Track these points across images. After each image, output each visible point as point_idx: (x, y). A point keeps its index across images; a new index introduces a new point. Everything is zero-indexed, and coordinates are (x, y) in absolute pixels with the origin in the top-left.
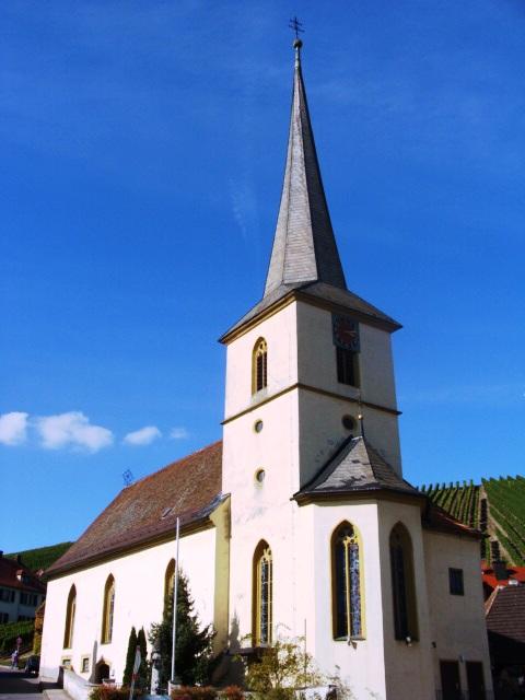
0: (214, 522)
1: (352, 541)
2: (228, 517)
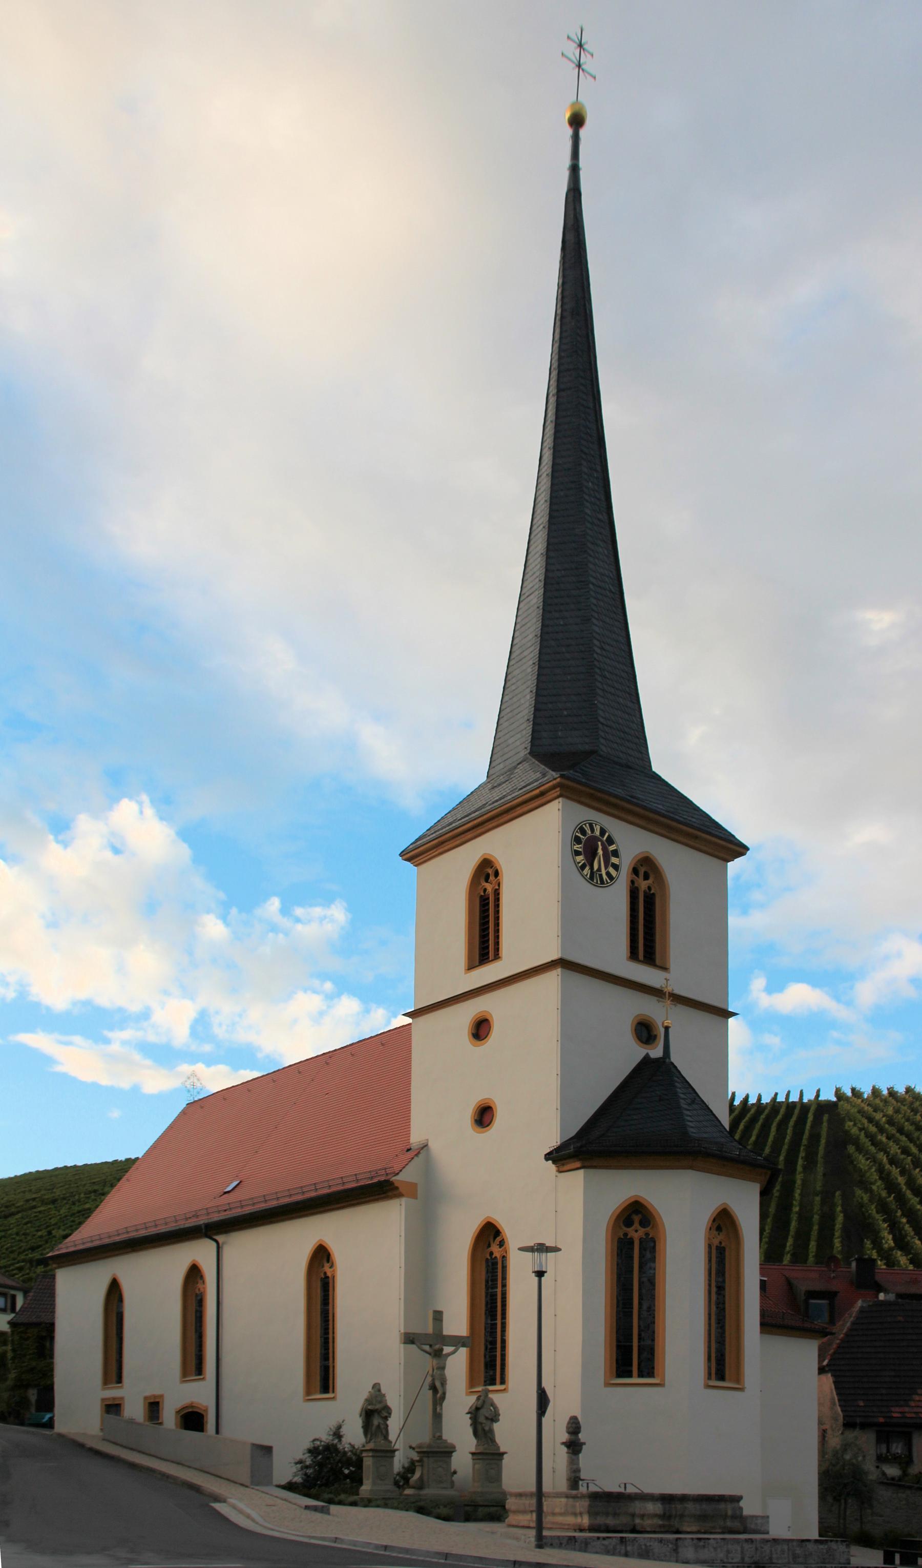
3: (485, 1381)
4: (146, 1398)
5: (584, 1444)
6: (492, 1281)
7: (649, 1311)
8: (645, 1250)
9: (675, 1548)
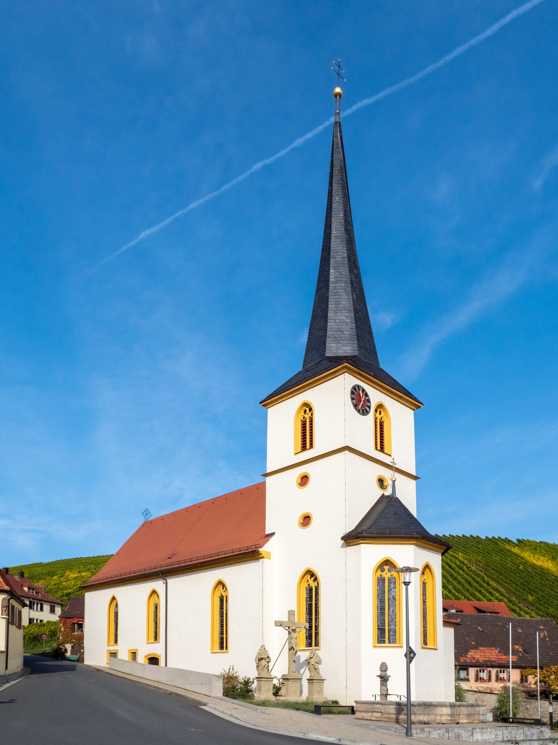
3: (306, 645)
4: (129, 650)
5: (390, 676)
6: (309, 598)
7: (393, 612)
8: (391, 583)
9: (472, 734)
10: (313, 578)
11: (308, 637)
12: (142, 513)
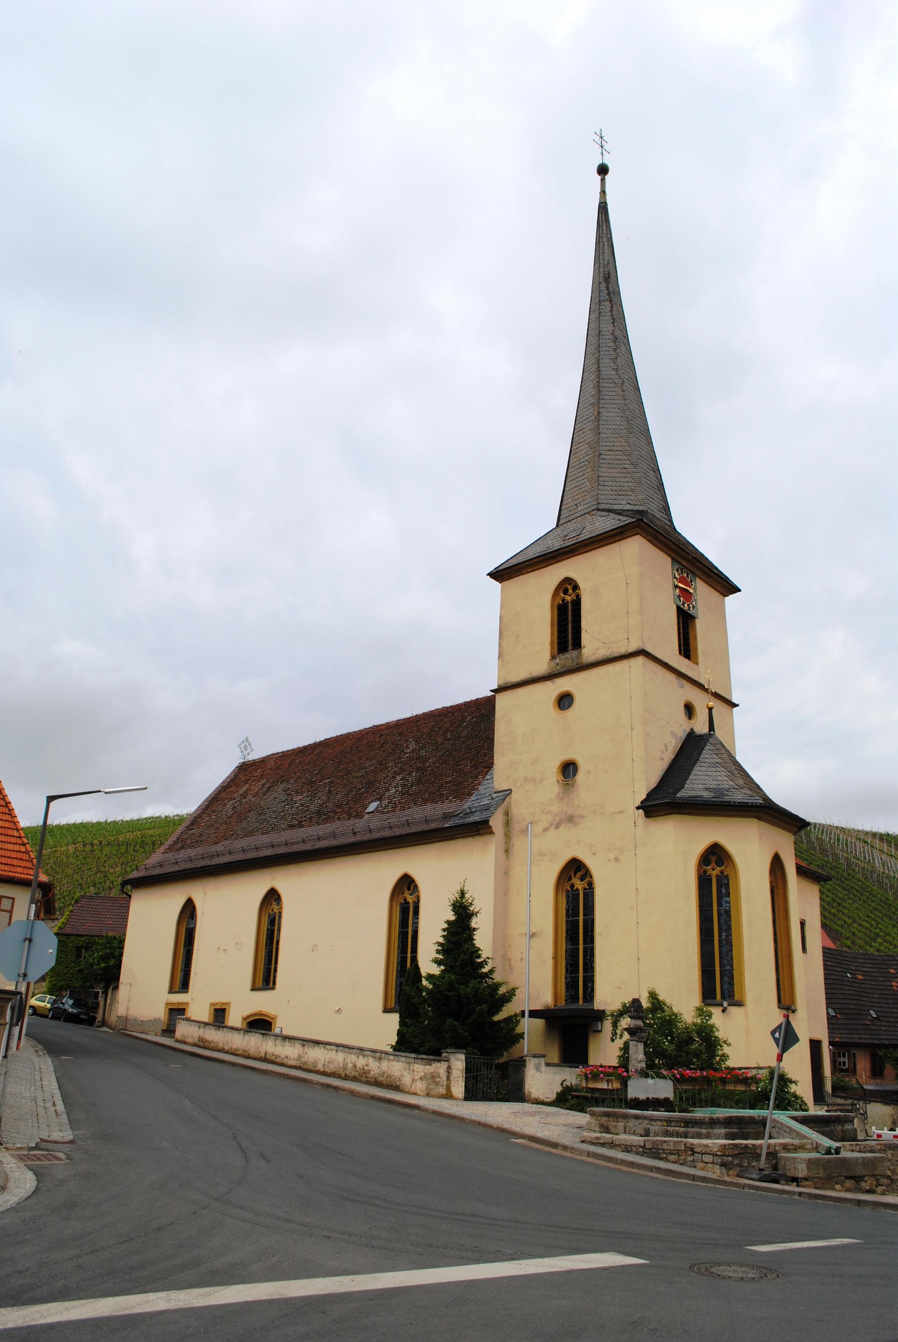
0: (494, 829)
1: (722, 872)
2: (508, 823)
4: (212, 1004)
10: (579, 874)
11: (570, 984)
12: (239, 746)
